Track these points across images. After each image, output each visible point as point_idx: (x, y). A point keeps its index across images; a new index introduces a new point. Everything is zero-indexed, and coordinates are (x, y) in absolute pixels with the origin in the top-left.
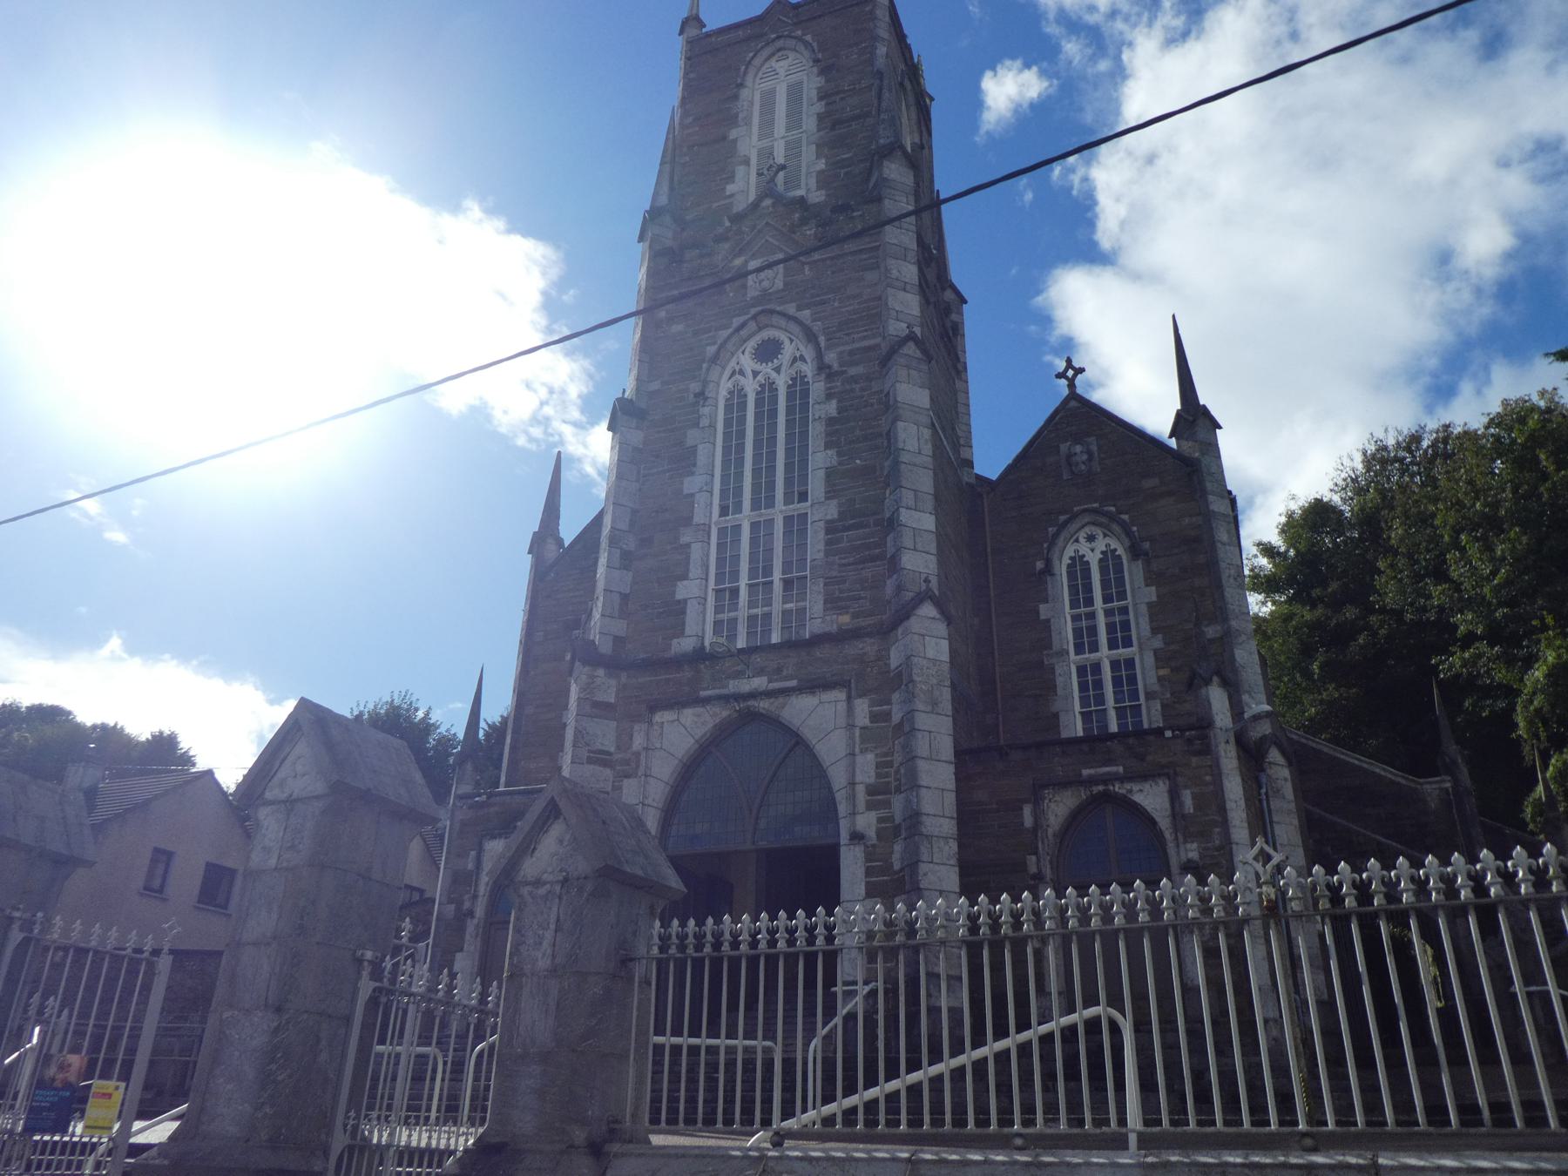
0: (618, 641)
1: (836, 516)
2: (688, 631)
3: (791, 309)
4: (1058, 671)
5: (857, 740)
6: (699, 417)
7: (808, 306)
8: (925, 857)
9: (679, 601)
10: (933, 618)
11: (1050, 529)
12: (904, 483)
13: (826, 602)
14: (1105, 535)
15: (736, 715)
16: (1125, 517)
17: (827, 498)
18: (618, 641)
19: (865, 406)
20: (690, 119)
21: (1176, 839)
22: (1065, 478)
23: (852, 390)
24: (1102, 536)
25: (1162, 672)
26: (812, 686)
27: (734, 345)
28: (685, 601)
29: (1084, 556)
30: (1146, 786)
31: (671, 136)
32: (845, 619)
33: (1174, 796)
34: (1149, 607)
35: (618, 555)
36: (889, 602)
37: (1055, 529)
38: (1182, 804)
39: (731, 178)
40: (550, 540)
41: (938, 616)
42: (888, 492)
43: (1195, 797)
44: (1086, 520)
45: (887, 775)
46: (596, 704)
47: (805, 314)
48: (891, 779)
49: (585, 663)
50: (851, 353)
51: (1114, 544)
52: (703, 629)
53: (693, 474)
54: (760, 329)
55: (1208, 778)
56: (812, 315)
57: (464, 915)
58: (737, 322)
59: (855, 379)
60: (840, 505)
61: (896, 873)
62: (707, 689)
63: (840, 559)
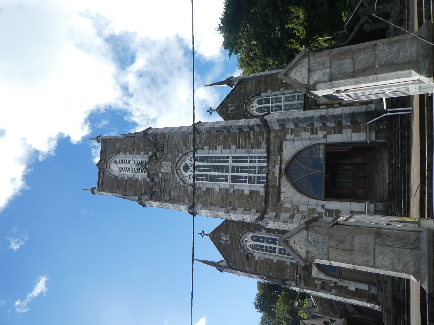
0: (257, 212)
1: (235, 146)
3: (177, 160)
7: (178, 155)
9: (250, 193)
11: (248, 116)
13: (258, 148)
14: (253, 103)
15: (285, 175)
16: (249, 97)
17: (230, 149)
19: (208, 139)
23: (203, 142)
24: (253, 104)
26: (281, 151)
27: (182, 177)
29: (257, 108)
36: (261, 130)
37: (248, 115)
40: (220, 264)
44: (248, 107)
45: (308, 129)
47: (180, 155)
48: (309, 128)
51: (255, 101)
53: (214, 189)
54: (180, 169)
57: (336, 285)
58: (176, 175)
59: (200, 142)
60: (232, 145)
61: (336, 125)
63: (247, 145)
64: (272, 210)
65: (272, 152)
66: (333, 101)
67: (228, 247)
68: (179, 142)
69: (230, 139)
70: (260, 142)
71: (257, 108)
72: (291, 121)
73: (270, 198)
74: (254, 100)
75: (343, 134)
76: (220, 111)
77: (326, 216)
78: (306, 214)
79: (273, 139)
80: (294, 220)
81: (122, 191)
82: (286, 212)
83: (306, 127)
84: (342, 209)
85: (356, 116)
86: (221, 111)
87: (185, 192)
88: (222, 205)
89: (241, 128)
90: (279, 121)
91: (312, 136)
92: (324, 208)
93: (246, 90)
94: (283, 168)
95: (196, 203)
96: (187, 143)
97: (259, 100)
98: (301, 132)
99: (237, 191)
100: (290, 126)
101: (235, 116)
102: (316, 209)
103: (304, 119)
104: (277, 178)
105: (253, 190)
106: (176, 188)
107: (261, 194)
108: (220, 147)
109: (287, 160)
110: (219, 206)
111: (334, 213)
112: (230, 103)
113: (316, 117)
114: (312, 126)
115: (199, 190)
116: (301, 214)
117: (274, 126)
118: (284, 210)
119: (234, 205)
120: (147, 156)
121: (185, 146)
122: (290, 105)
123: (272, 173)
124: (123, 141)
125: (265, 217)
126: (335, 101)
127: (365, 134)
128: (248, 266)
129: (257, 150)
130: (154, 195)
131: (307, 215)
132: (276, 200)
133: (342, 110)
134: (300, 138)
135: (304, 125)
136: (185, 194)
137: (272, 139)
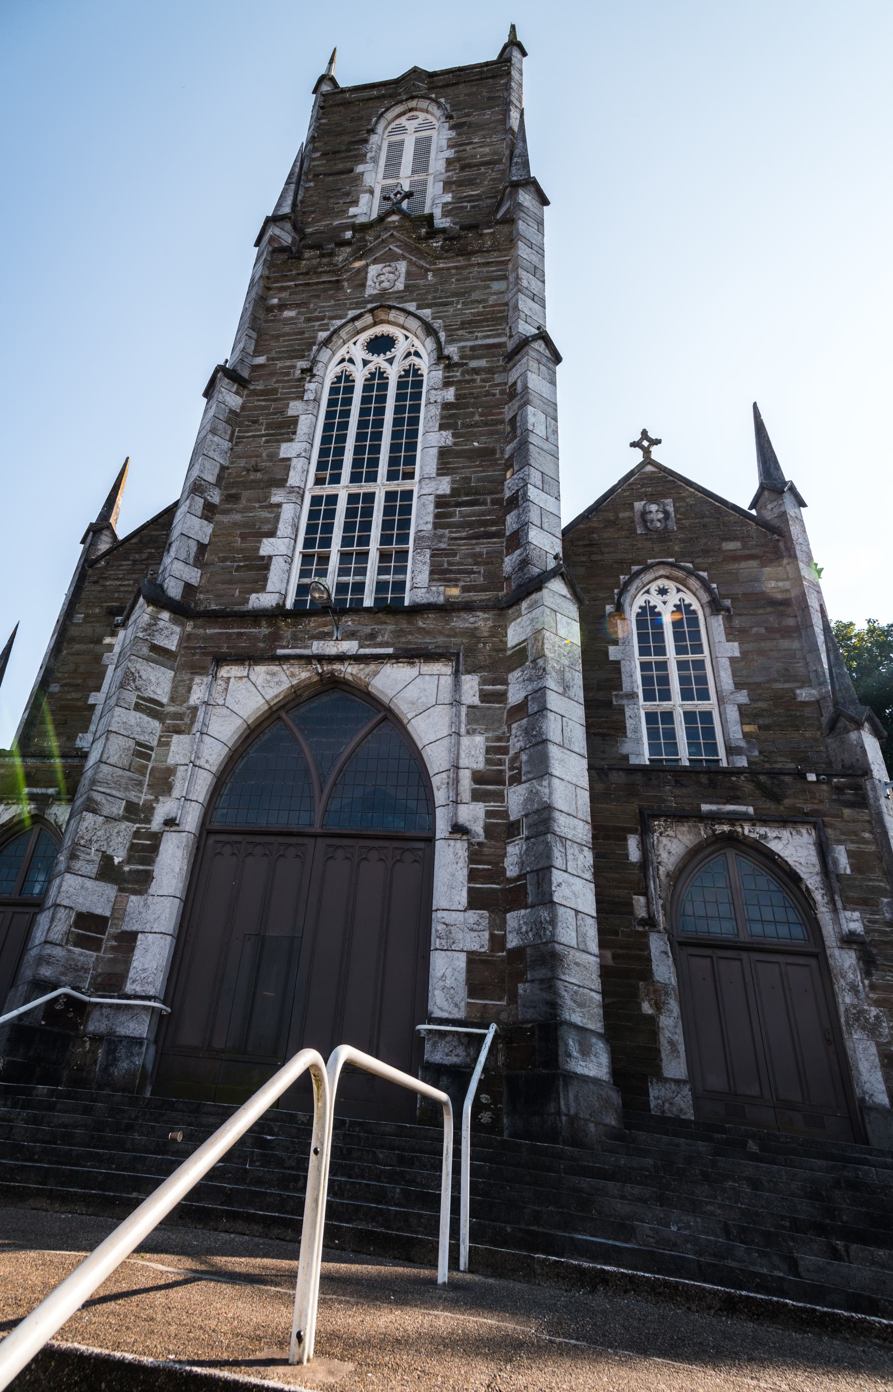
1: (448, 492)
2: (270, 587)
3: (412, 307)
4: (628, 713)
5: (463, 718)
6: (304, 391)
7: (428, 306)
8: (558, 862)
9: (263, 558)
10: (564, 596)
11: (622, 577)
12: (532, 462)
13: (432, 572)
15: (316, 678)
16: (704, 574)
17: (438, 475)
18: (188, 588)
20: (318, 154)
21: (832, 901)
22: (639, 532)
24: (675, 590)
25: (747, 728)
28: (270, 558)
29: (655, 607)
30: (785, 834)
31: (297, 170)
32: (455, 592)
33: (823, 851)
34: (731, 662)
35: (201, 505)
36: (508, 579)
37: (627, 577)
38: (836, 862)
39: (355, 203)
41: (569, 596)
42: (508, 474)
43: (850, 854)
45: (501, 763)
46: (155, 648)
47: (426, 313)
48: (506, 767)
49: (150, 601)
50: (473, 348)
51: (689, 598)
52: (286, 590)
53: (291, 440)
54: (375, 324)
55: (867, 835)
56: (433, 313)
58: (351, 314)
59: (476, 371)
60: (453, 482)
62: (287, 647)
63: (450, 532)
64: (186, 639)
65: (409, 623)
66: (663, 895)
67: (153, 551)
68: (479, 302)
69: (475, 472)
70: (457, 580)
71: (655, 607)
72: (535, 685)
73: (232, 628)
74: (694, 594)
75: (465, 911)
76: (645, 473)
77: (137, 834)
78: (155, 760)
79: (467, 625)
80: (133, 713)
81: (318, 166)
82: (174, 689)
83: (507, 753)
84: (150, 897)
85: (542, 973)
86: (642, 479)
87: (291, 351)
88: (230, 474)
89: (518, 501)
90: (536, 639)
91: (465, 777)
92: (167, 829)
93: (735, 558)
94: (343, 669)
95: (246, 392)
96: (474, 327)
97: (694, 612)
98: (490, 735)
99: (272, 515)
100: (518, 686)
101: (621, 529)
102: (170, 796)
103: (539, 739)
104: (305, 647)
105: (272, 567)
106: (309, 320)
107: (253, 596)
108: (450, 441)
109: (373, 682)
110: (226, 463)
111: (141, 867)
112: (677, 505)
113: (547, 791)
114: (511, 777)
115: (293, 393)
116: (159, 740)
117: (520, 623)
118: (184, 681)
119: (226, 512)
120: (438, 212)
121: (463, 323)
122: (671, 735)
123: (326, 629)
124: (500, 127)
125: (158, 613)
126: (661, 902)
127: (459, 1014)
128: (87, 616)
129: (426, 570)
130: (289, 258)
131: (150, 765)
132: (224, 650)
133: (577, 912)
134: (463, 730)
135: (516, 744)
136: (283, 351)
137: (463, 622)
